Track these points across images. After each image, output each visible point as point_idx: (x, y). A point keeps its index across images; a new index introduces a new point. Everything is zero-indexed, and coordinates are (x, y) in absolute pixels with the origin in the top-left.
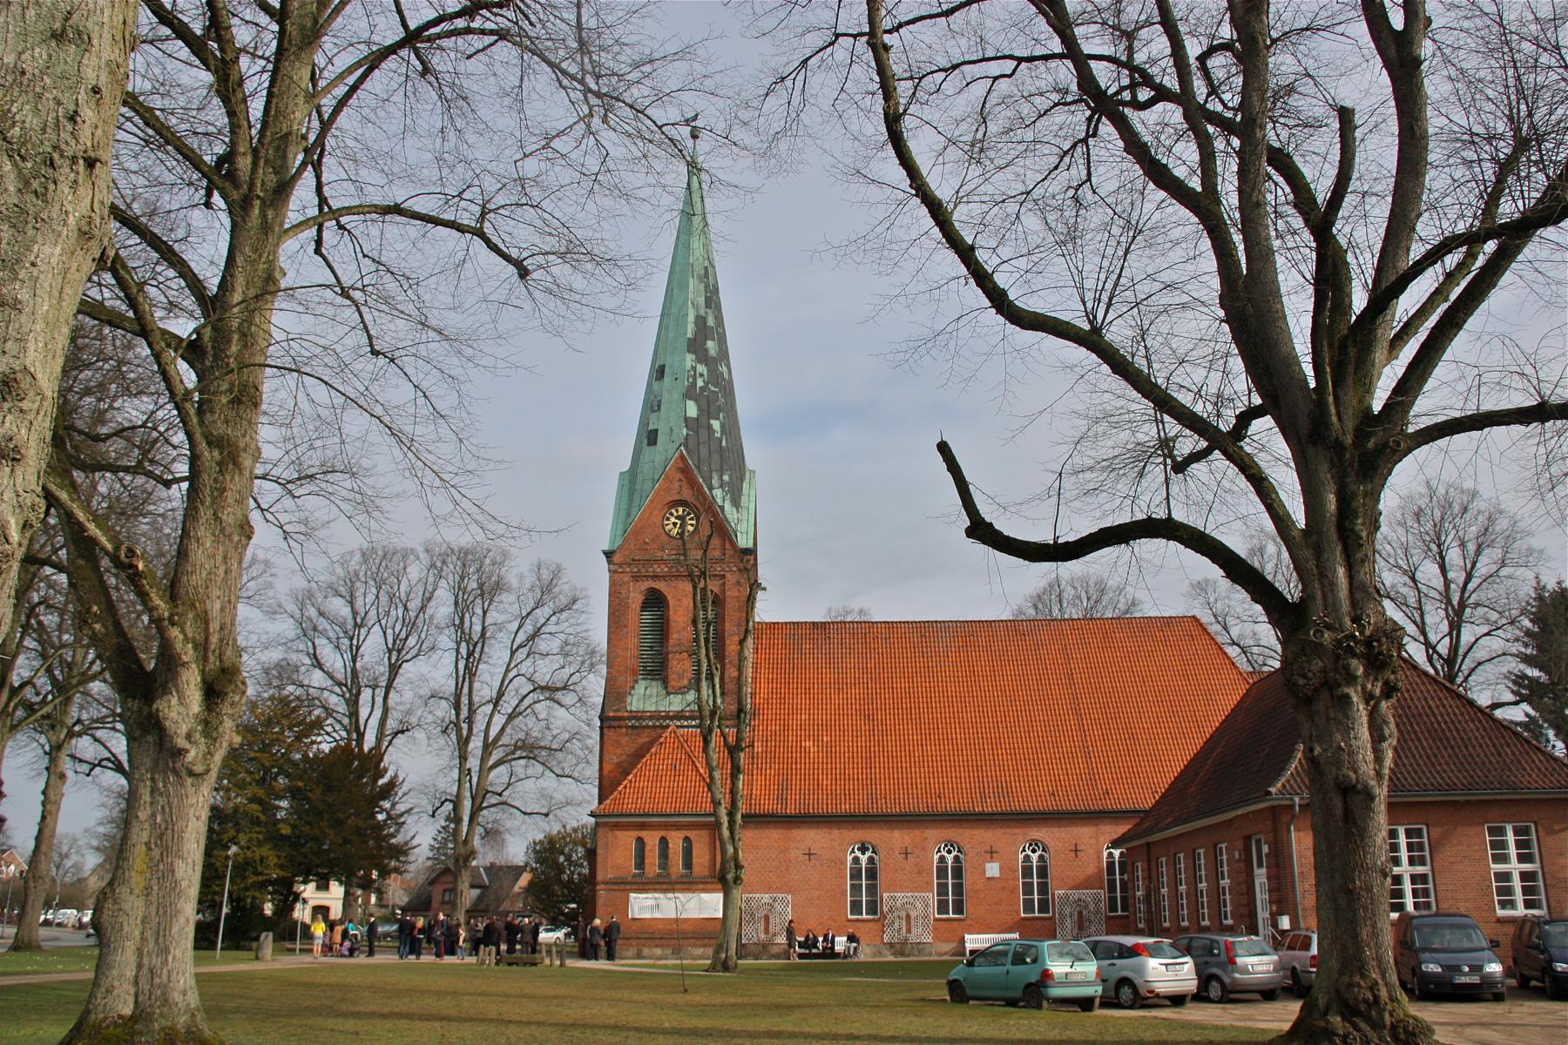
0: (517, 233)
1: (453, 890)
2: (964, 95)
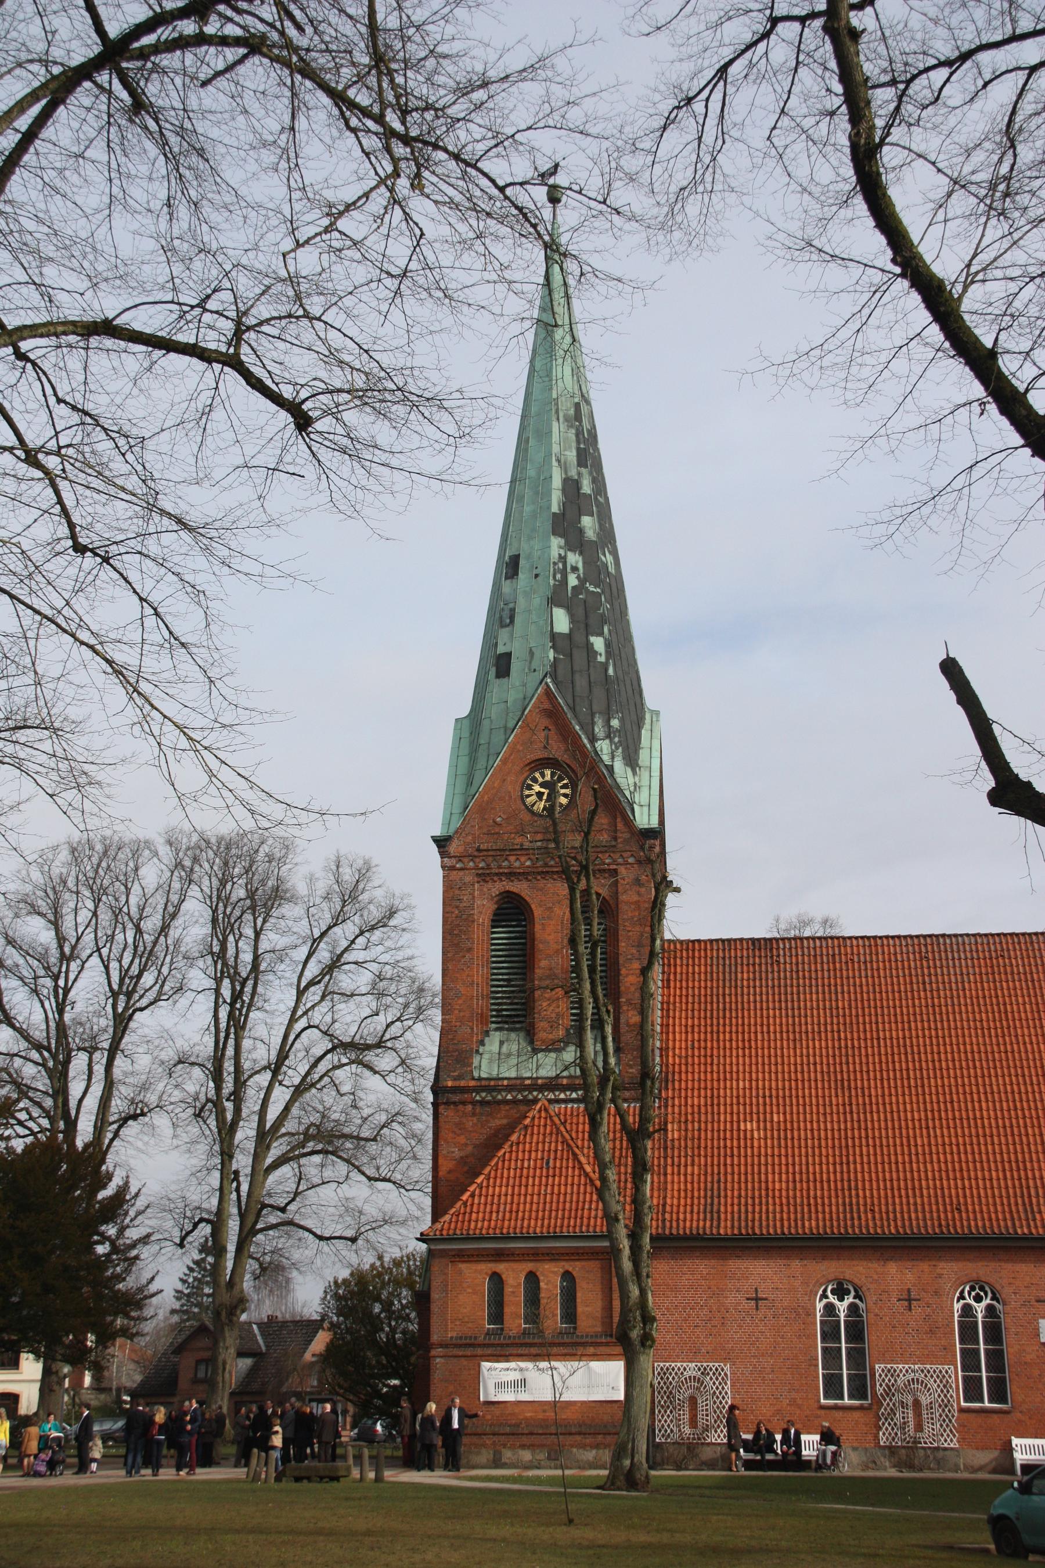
0: (294, 364)
1: (211, 1361)
2: (978, 104)
